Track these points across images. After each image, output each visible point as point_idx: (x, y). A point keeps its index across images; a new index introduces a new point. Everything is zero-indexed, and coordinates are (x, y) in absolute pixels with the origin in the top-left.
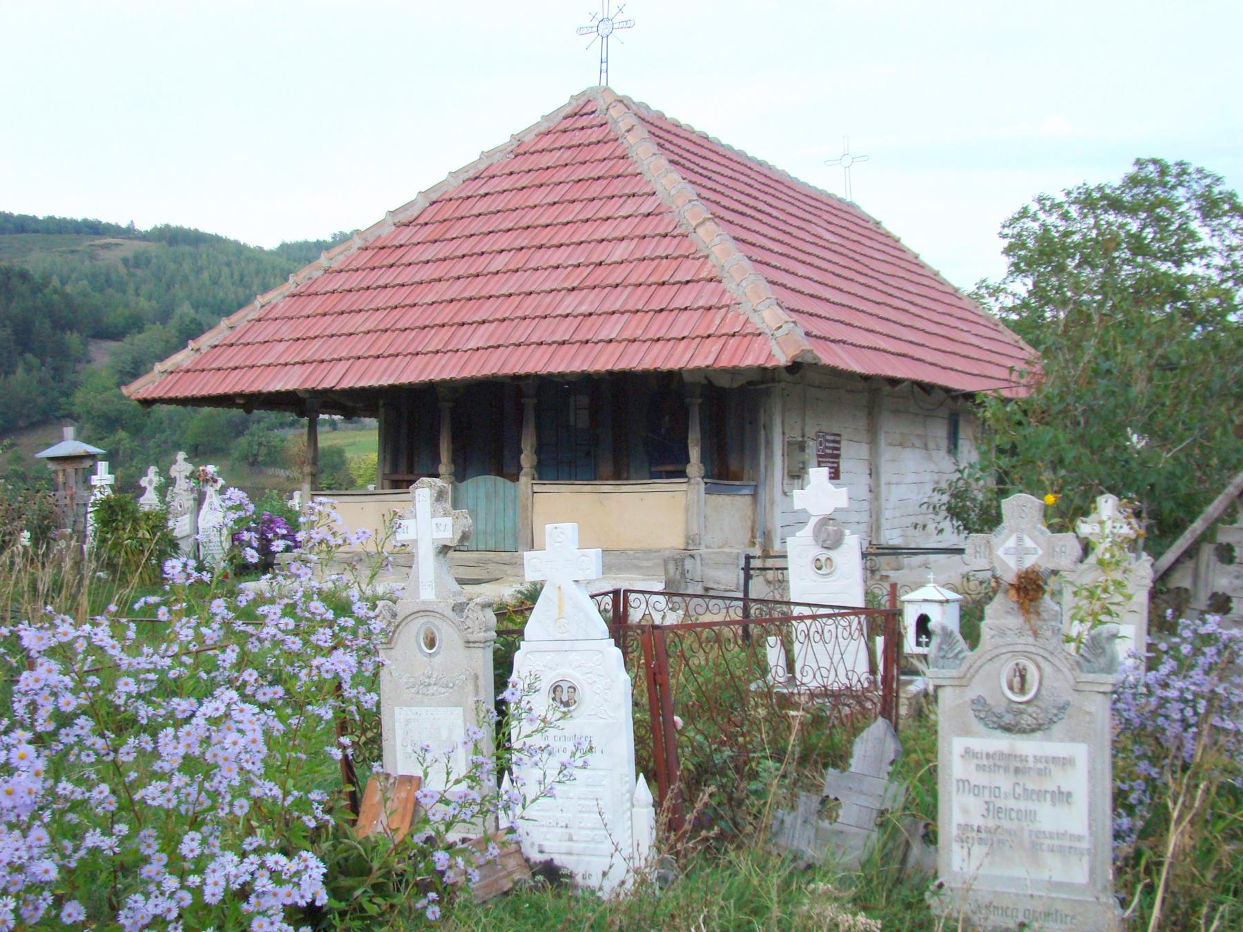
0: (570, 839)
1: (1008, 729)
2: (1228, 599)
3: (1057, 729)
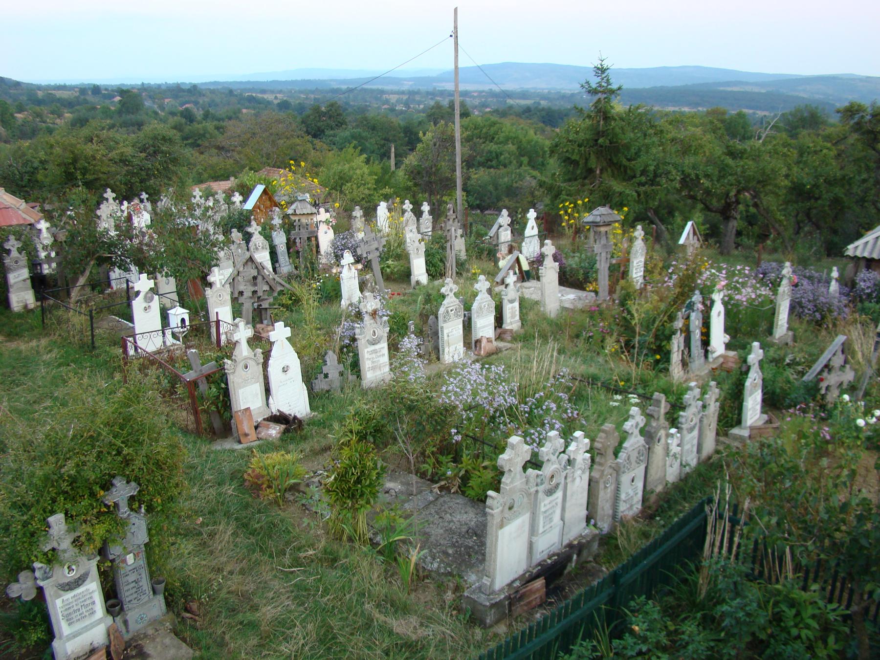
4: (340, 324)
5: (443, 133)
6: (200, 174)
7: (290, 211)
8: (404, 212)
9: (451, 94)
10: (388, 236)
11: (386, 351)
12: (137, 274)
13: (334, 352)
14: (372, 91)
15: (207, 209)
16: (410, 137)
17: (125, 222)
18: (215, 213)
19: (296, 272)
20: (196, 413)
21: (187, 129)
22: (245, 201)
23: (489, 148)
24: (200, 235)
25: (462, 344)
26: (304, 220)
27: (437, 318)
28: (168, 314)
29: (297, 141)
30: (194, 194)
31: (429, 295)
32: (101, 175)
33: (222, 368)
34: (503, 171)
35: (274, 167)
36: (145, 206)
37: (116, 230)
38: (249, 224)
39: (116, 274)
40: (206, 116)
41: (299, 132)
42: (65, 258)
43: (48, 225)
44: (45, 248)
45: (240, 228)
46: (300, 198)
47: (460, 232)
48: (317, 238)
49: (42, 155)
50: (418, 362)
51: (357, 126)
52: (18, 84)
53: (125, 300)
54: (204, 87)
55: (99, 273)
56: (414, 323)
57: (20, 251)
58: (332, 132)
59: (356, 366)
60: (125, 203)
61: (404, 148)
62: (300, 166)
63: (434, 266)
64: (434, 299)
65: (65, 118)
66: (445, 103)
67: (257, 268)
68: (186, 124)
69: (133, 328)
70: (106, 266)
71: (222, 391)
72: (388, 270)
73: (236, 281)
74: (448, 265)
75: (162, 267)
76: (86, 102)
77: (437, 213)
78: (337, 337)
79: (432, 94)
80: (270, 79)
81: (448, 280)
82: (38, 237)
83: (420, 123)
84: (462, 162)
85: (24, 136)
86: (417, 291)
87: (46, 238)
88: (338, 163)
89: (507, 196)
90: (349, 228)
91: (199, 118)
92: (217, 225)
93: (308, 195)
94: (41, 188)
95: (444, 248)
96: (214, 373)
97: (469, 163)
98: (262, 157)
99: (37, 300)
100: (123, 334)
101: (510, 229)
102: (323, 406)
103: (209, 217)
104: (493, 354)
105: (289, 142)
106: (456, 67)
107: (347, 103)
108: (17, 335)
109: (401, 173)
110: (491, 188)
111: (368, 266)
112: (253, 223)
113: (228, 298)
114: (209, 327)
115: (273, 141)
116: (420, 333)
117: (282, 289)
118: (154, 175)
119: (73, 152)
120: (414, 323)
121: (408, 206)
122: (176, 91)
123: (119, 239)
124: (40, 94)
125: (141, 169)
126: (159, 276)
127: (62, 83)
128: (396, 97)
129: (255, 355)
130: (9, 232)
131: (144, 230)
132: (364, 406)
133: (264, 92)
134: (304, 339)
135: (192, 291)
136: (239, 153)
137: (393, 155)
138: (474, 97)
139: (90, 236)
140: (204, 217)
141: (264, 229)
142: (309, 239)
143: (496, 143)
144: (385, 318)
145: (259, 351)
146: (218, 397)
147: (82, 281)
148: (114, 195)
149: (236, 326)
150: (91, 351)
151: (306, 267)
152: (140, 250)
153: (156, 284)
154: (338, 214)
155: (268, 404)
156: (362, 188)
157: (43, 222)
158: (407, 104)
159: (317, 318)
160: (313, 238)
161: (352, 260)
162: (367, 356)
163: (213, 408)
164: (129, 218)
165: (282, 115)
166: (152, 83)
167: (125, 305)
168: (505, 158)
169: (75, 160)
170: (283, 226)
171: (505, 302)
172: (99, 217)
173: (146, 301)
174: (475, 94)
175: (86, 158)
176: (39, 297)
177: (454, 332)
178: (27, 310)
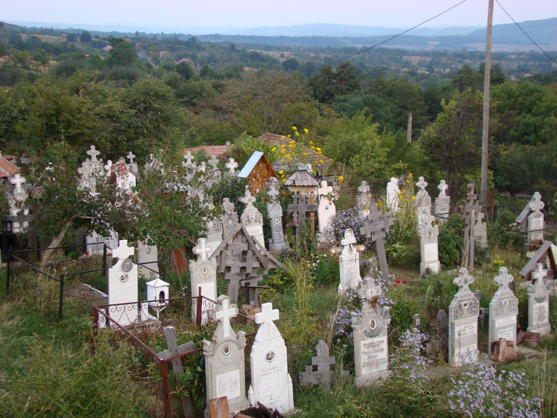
0: (272, 399)
1: (371, 337)
2: (227, 267)
3: (381, 334)
4: (334, 311)
5: (469, 101)
6: (193, 136)
7: (288, 182)
8: (417, 189)
9: (482, 56)
10: (397, 216)
11: (385, 346)
12: (116, 240)
13: (326, 342)
14: (391, 51)
15: (199, 174)
16: (431, 105)
17: (108, 183)
18: (207, 179)
19: (290, 250)
20: (166, 398)
21: (183, 85)
22: (240, 168)
23: (526, 120)
24: (189, 202)
25: (475, 346)
26: (303, 193)
27: (447, 312)
28: (146, 286)
29: (303, 105)
30: (186, 157)
31: (440, 286)
32: (85, 130)
33: (200, 349)
34: (541, 147)
35: (275, 133)
36: (131, 167)
37: (98, 191)
38: (243, 194)
39: (93, 238)
40: (205, 72)
41: (305, 96)
42: (39, 217)
43: (23, 180)
45: (233, 198)
46: (300, 168)
47: (481, 216)
48: (316, 213)
50: (420, 361)
51: (371, 91)
53: (100, 267)
54: (202, 40)
55: (74, 236)
56: (422, 317)
58: (342, 97)
59: (349, 360)
60: (110, 162)
61: (424, 118)
62: (304, 132)
63: (448, 252)
64: (445, 291)
65: (49, 66)
66: (475, 66)
67: (247, 242)
68: (182, 80)
69: (107, 298)
70: (83, 229)
71: (197, 375)
72: (395, 255)
73: (223, 254)
74: (464, 253)
75: (145, 233)
76: (74, 49)
77: (457, 194)
78: (331, 325)
79: (461, 56)
80: (277, 35)
81: (463, 270)
82: (12, 193)
83: (445, 89)
84: (490, 136)
86: (427, 281)
87: (20, 194)
88: (347, 132)
89: (545, 178)
90: (353, 204)
91: (196, 74)
92: (207, 192)
93: (310, 166)
94: (18, 140)
95: (461, 234)
96: (190, 354)
97: (498, 137)
98: (263, 121)
100: (95, 304)
101: (543, 215)
102: (310, 402)
103: (201, 183)
104: (513, 360)
105: (293, 106)
106: (490, 25)
107: (362, 65)
109: (417, 146)
110: (524, 167)
111: (371, 248)
112: (248, 193)
113: (213, 272)
114: (190, 304)
115: (276, 105)
116: (426, 328)
117: (274, 267)
118: (143, 134)
119: (56, 103)
120: (422, 317)
121: (422, 183)
122: (174, 43)
123: (100, 201)
124: (24, 37)
125: (129, 127)
126: (140, 243)
127: (49, 27)
128: (419, 58)
129: (237, 338)
131: (129, 192)
132: (356, 407)
133: (269, 48)
134: (293, 325)
135: (175, 263)
136: (238, 115)
137: (410, 125)
138: (512, 60)
139: (68, 195)
140: (195, 182)
141: (259, 200)
142: (308, 214)
143: (535, 115)
144: (387, 308)
145: (243, 333)
146: (192, 382)
147: (55, 243)
148: (98, 153)
149: (219, 303)
150: (57, 321)
151: (302, 245)
152: (122, 215)
153: (136, 252)
154: (342, 188)
155: (247, 395)
156: (371, 161)
157: (18, 176)
158: (430, 68)
159: (310, 302)
160: (312, 214)
161: (353, 240)
162: (363, 349)
163: (186, 394)
164: (113, 179)
165: (288, 75)
166: (148, 32)
167: (100, 272)
168: (545, 133)
169: (58, 113)
170: (279, 198)
171: (531, 300)
172: (80, 176)
173: (123, 270)
174: (513, 57)
175: (71, 111)
177: (467, 330)
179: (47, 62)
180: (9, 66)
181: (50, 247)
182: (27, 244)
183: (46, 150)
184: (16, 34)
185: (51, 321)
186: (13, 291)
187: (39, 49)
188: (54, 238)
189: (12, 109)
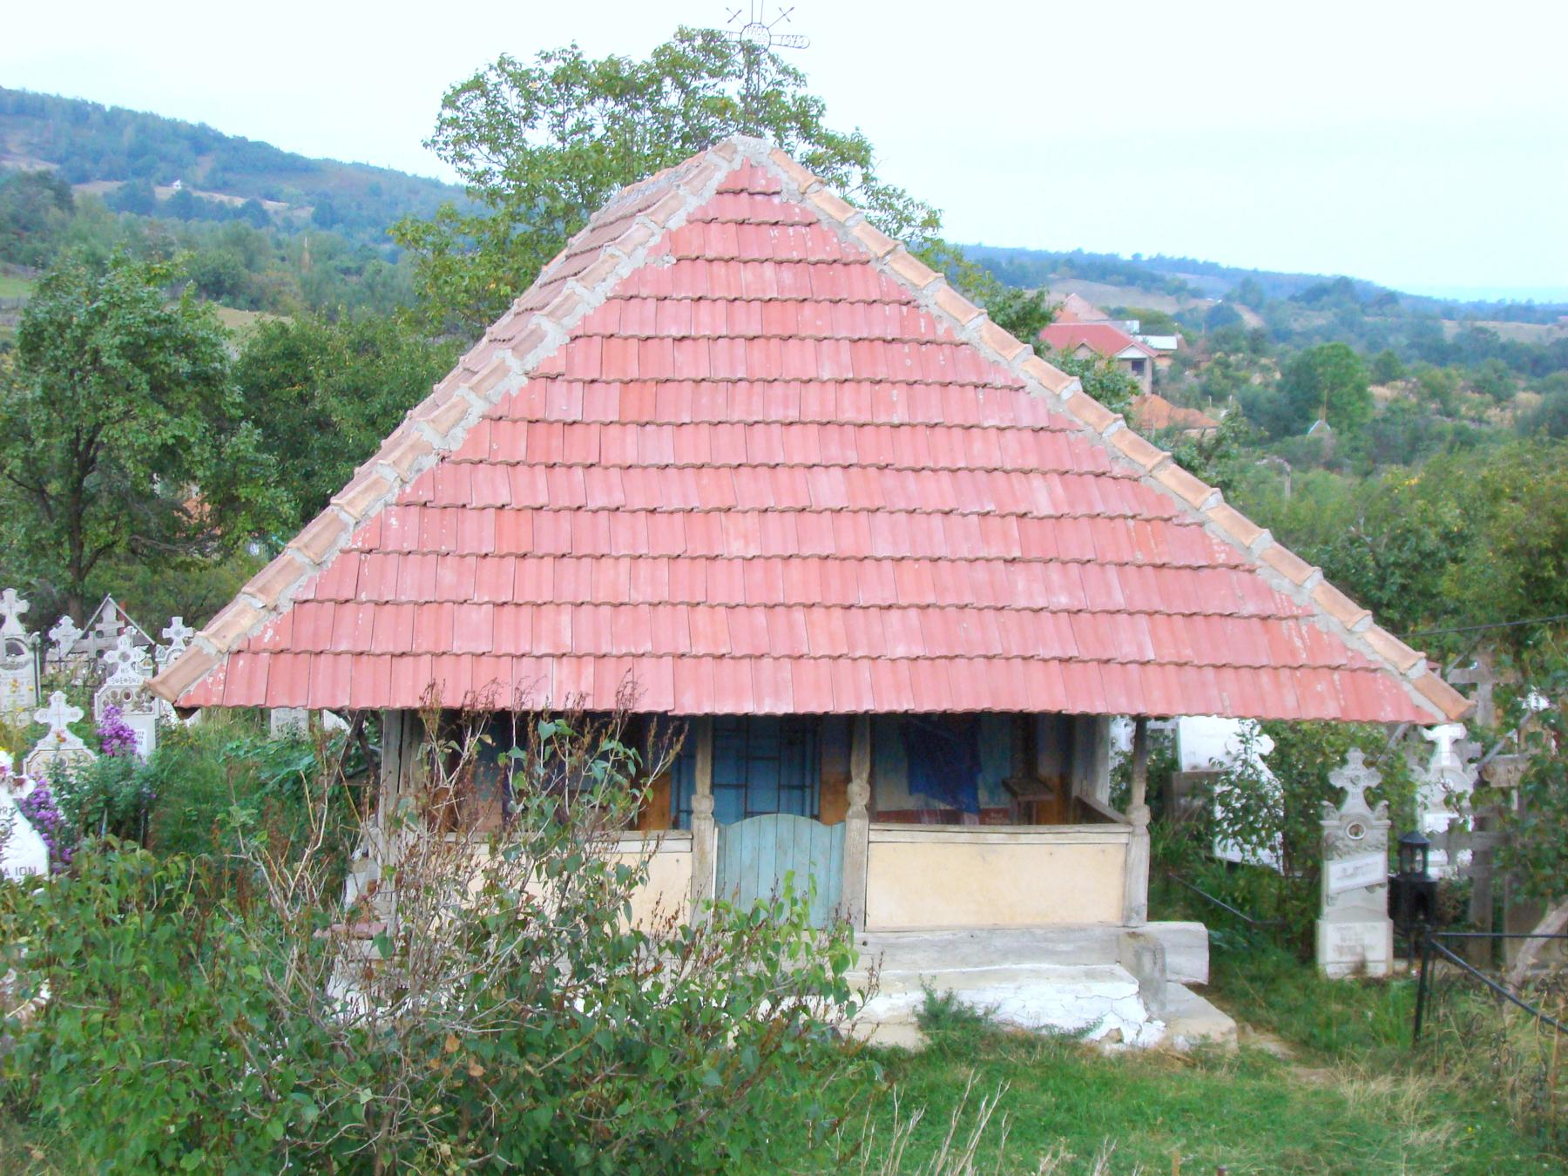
44: (1451, 801)
49: (1450, 514)
52: (1389, 299)
57: (1372, 797)
82: (1424, 762)
85: (1411, 449)
99: (1398, 953)
108: (1328, 1048)
124: (1450, 330)
130: (1353, 739)
176: (1409, 943)
178: (1364, 983)
179: (1509, 396)
180: (1403, 410)
181: (1537, 931)
182: (1464, 912)
183: (1540, 653)
184: (1429, 322)
185: (1544, 1149)
186: (1433, 1043)
187: (1490, 359)
188: (1551, 905)
189: (1425, 529)
